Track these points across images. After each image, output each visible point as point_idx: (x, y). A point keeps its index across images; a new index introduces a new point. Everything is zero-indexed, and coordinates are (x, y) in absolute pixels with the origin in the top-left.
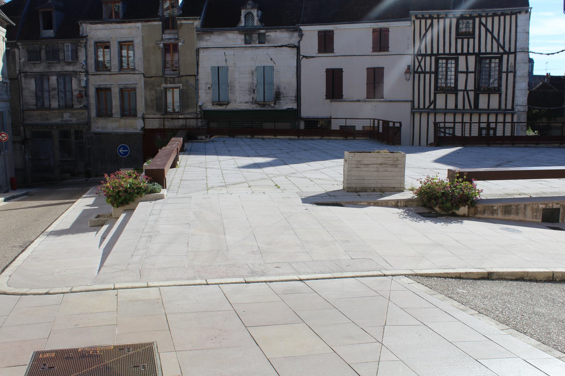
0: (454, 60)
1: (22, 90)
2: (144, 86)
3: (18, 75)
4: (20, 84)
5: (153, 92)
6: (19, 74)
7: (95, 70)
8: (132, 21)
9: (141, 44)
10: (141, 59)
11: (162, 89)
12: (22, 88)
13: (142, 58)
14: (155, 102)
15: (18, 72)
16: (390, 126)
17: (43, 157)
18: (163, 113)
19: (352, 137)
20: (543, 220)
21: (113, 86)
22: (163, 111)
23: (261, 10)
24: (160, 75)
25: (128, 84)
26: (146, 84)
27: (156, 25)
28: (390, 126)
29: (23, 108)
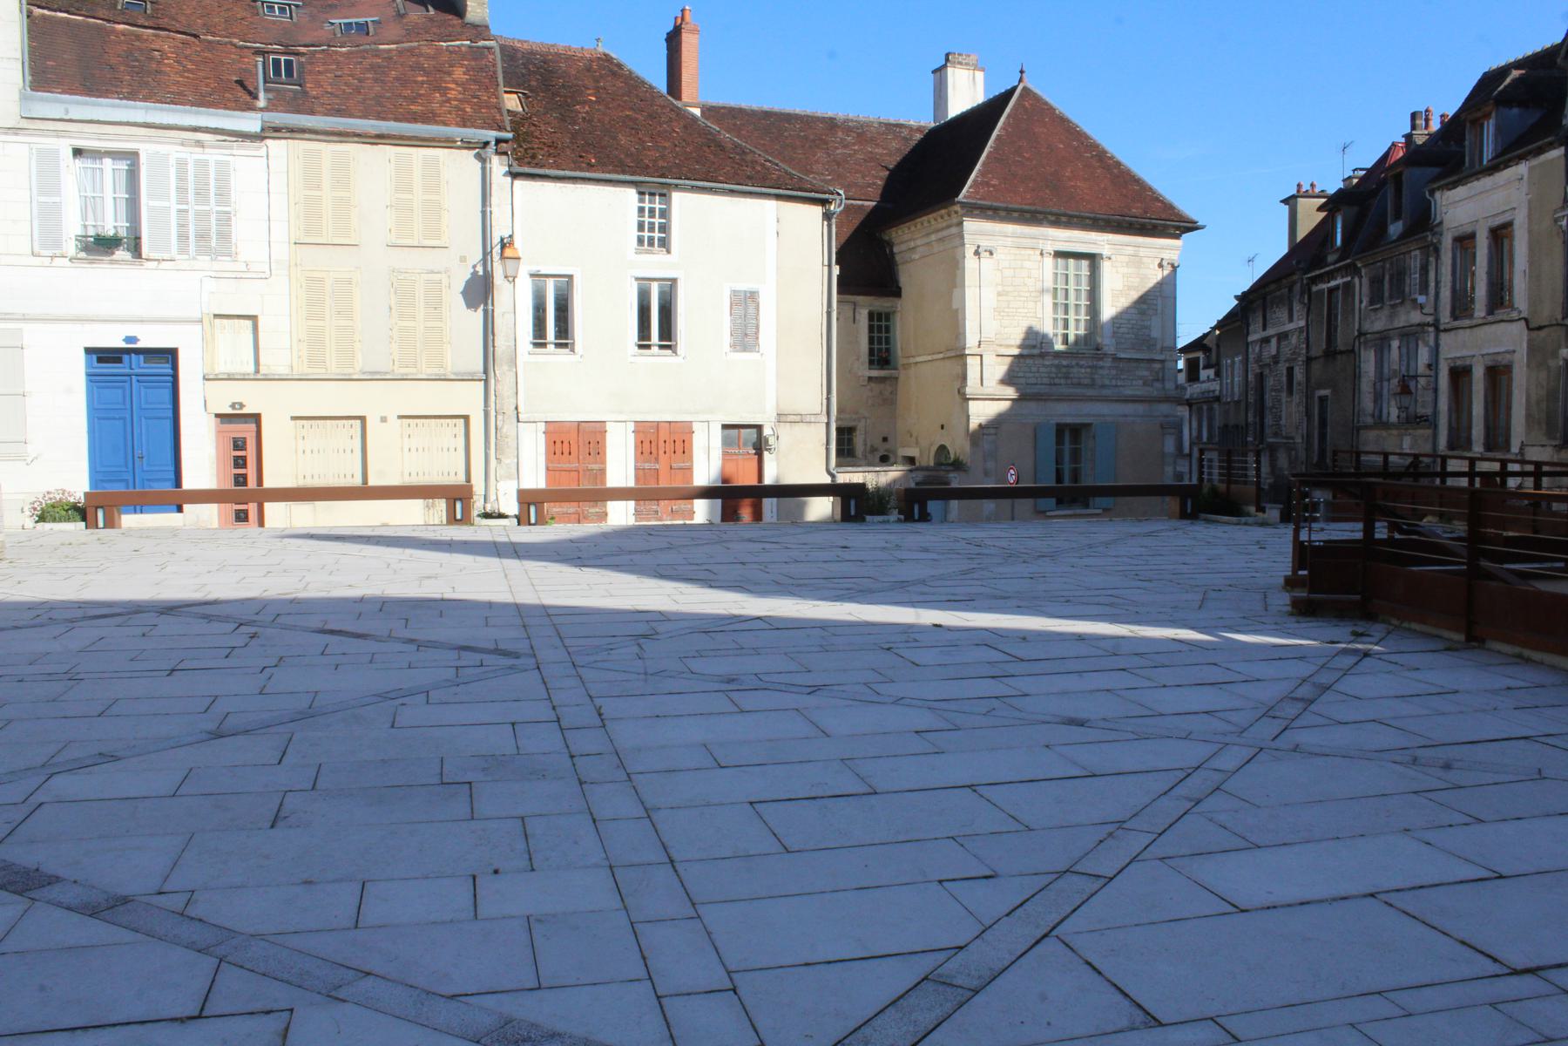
0: (1362, 538)
1: (1360, 376)
2: (1528, 354)
3: (1354, 342)
4: (1357, 363)
5: (1543, 375)
6: (1357, 336)
7: (1451, 317)
8: (1510, 160)
9: (1526, 226)
10: (1525, 271)
11: (1561, 363)
12: (1360, 372)
13: (1527, 271)
14: (1544, 406)
15: (1356, 333)
16: (1377, 536)
17: (1511, 534)
18: (1557, 443)
19: (1398, 539)
20: (469, 123)
21: (1475, 359)
22: (1558, 435)
23: (1364, 534)
24: (1556, 320)
25: (1498, 353)
26: (1532, 349)
27: (1553, 160)
28: (1377, 536)
29: (1358, 422)
